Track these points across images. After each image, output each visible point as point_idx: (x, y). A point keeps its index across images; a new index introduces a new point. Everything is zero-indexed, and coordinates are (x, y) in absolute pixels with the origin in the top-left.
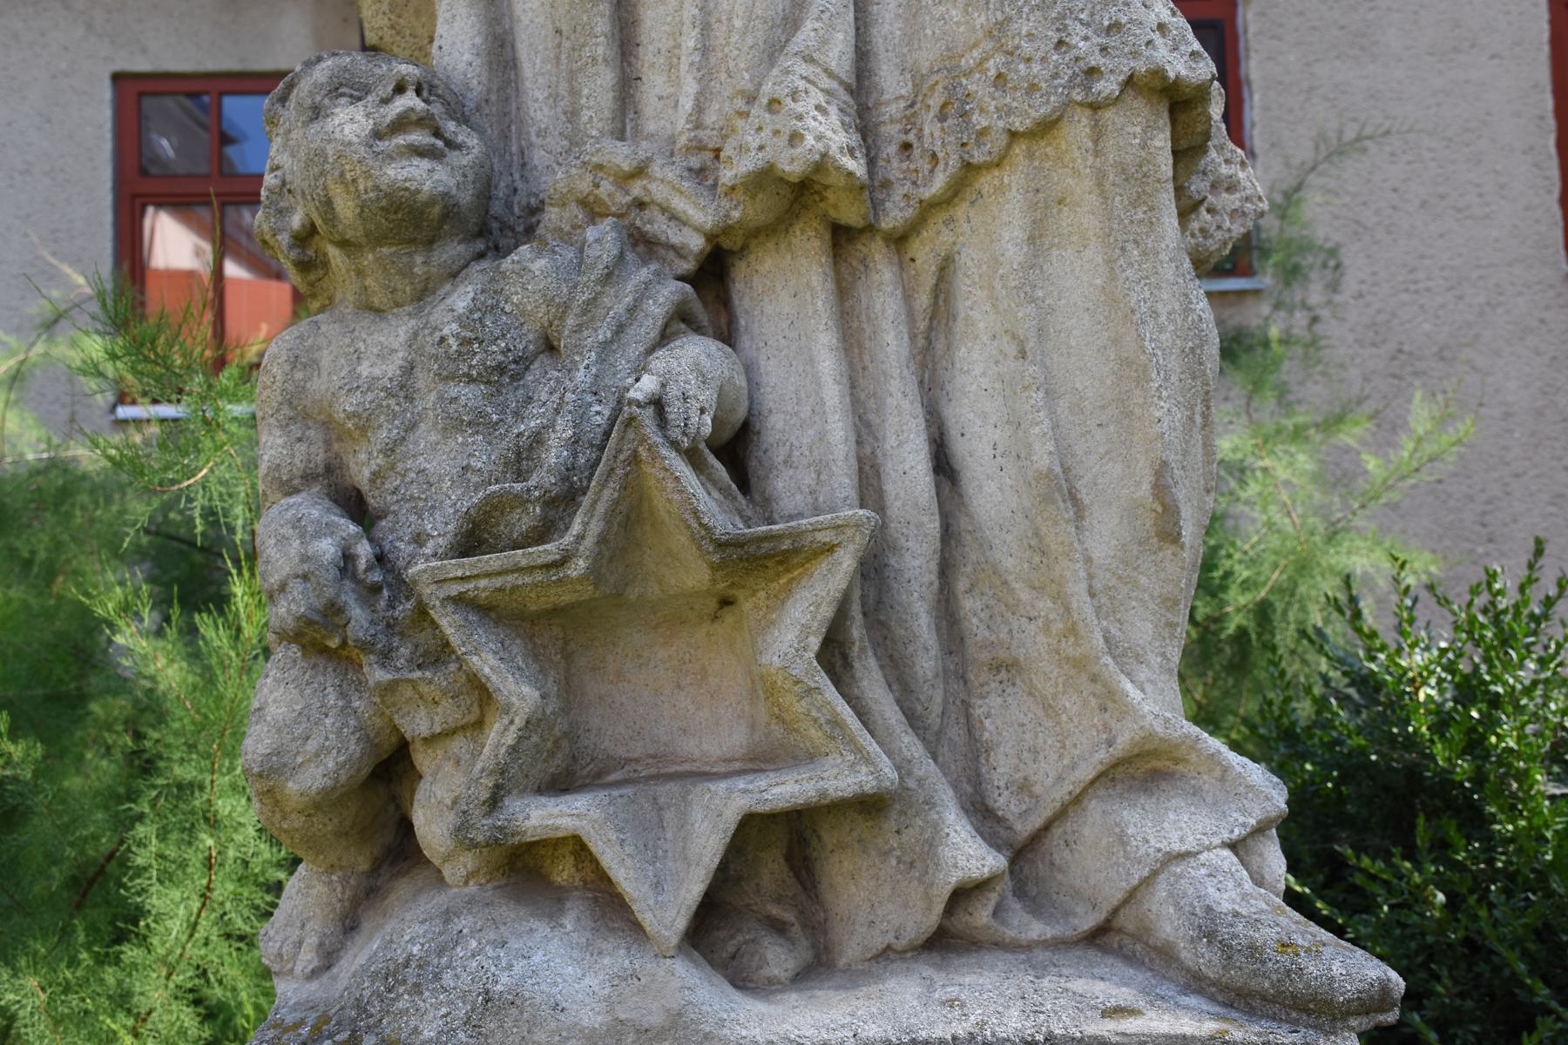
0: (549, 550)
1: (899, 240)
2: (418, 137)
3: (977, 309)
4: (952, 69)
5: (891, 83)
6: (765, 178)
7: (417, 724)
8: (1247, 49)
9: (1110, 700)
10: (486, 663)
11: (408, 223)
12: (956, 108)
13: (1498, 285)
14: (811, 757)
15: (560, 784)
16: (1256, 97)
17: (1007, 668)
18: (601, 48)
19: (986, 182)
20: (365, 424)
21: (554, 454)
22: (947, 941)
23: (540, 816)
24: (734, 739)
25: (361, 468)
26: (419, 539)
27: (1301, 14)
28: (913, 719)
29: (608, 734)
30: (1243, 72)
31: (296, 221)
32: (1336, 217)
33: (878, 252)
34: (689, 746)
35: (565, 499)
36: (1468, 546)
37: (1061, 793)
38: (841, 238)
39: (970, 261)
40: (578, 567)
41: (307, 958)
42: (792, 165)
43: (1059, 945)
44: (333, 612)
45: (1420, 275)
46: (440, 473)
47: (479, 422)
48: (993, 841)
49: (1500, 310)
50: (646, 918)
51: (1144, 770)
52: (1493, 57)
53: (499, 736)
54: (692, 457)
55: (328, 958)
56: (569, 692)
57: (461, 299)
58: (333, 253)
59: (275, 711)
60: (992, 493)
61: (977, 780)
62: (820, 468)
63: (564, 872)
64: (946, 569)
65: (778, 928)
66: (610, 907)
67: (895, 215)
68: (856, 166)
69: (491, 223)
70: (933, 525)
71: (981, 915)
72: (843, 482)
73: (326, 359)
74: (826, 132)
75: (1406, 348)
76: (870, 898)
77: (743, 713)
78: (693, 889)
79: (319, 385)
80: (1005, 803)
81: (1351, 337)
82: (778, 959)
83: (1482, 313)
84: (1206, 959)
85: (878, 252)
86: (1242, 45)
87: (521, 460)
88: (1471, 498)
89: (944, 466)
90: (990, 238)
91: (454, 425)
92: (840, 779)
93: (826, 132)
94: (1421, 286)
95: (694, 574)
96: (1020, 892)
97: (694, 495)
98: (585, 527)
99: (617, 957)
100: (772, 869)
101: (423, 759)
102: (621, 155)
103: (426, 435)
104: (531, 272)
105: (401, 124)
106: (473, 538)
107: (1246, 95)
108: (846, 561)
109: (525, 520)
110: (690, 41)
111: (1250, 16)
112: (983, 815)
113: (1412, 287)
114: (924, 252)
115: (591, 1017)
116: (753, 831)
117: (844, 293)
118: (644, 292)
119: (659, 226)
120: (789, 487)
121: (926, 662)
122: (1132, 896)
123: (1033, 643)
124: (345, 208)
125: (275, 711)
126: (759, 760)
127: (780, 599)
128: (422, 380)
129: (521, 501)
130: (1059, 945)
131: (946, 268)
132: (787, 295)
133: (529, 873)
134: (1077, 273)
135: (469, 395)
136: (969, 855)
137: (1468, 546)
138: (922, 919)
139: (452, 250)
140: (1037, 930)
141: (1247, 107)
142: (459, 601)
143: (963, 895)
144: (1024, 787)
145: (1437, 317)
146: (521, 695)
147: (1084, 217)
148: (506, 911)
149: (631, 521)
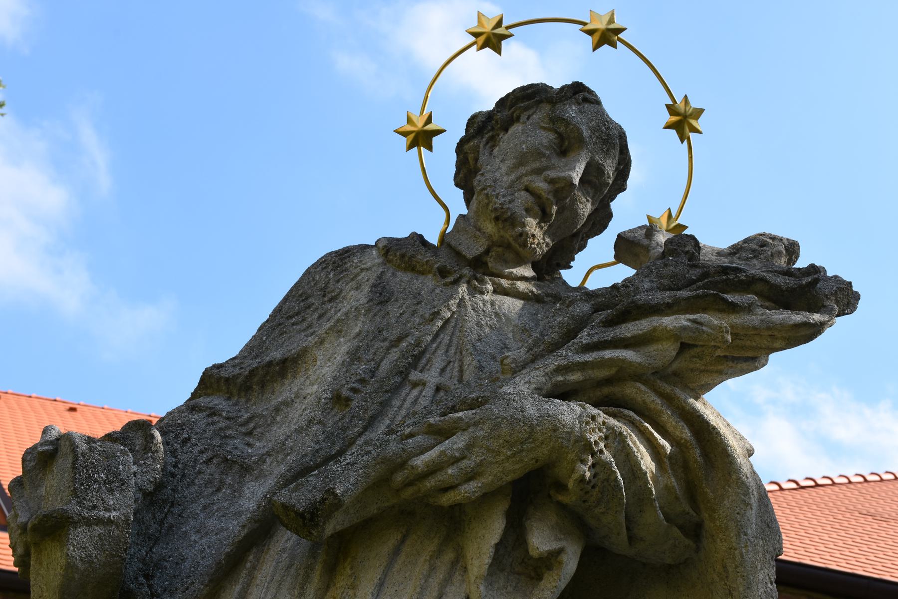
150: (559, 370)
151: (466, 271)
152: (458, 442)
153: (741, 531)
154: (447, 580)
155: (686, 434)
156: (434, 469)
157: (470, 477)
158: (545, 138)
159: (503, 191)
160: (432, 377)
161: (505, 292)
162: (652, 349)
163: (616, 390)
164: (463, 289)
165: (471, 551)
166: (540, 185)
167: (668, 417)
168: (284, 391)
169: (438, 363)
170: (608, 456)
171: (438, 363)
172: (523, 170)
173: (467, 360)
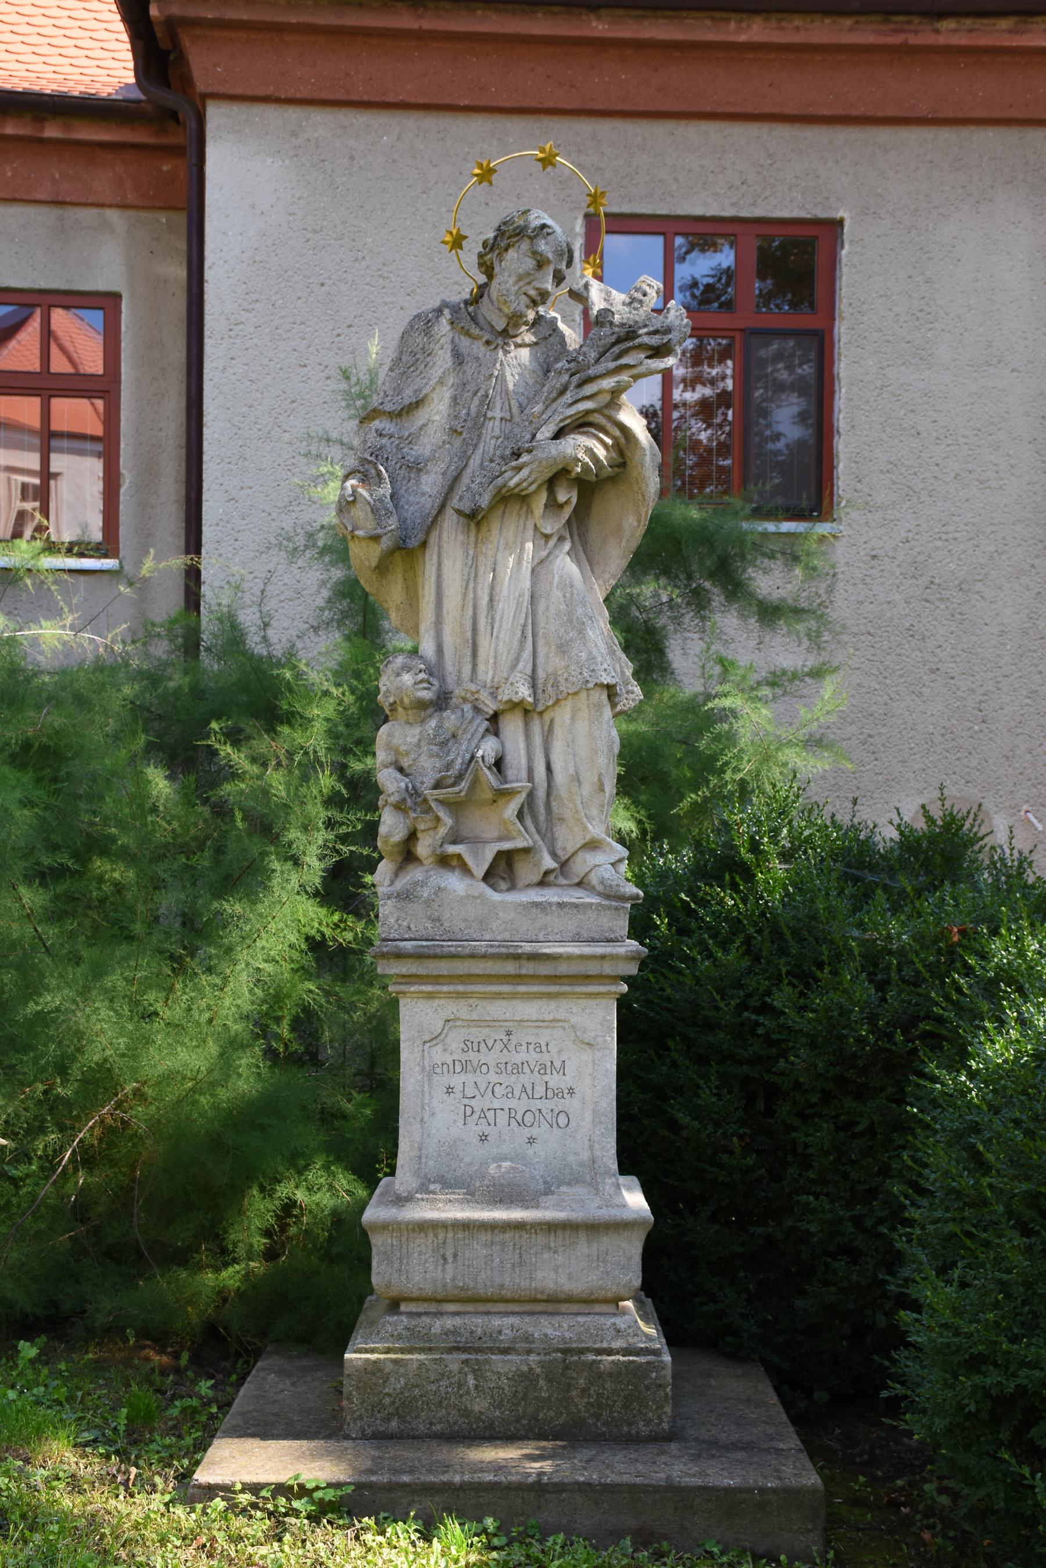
0: (457, 789)
1: (541, 713)
2: (425, 685)
3: (559, 732)
4: (555, 674)
5: (541, 674)
6: (510, 701)
7: (421, 826)
8: (840, 354)
9: (585, 829)
10: (441, 814)
11: (422, 705)
12: (556, 685)
13: (1004, 538)
14: (513, 839)
15: (454, 842)
16: (843, 391)
17: (561, 820)
18: (469, 659)
19: (562, 703)
20: (407, 753)
21: (457, 766)
22: (542, 883)
23: (452, 849)
24: (495, 834)
25: (405, 763)
26: (422, 783)
27: (880, 330)
28: (538, 831)
29: (465, 832)
30: (836, 372)
31: (391, 700)
32: (894, 483)
33: (536, 716)
34: (484, 835)
35: (460, 777)
36: (969, 724)
37: (571, 851)
38: (526, 712)
39: (557, 720)
40: (463, 794)
41: (387, 882)
42: (516, 699)
43: (569, 886)
44: (404, 800)
45: (951, 528)
46: (428, 768)
47: (437, 756)
48: (556, 861)
49: (1004, 557)
50: (475, 873)
51: (592, 845)
52: (1013, 370)
53: (442, 831)
54: (489, 768)
55: (392, 883)
56: (457, 821)
57: (433, 723)
58: (400, 709)
59: (389, 822)
60: (560, 778)
61: (553, 847)
62: (519, 770)
63: (454, 863)
64: (548, 795)
65: (503, 879)
66: (465, 870)
67: (540, 708)
68: (530, 700)
69: (442, 702)
70: (545, 785)
71: (552, 877)
72: (524, 774)
73: (397, 734)
74: (524, 692)
75: (937, 581)
76: (526, 872)
77: (498, 828)
78: (486, 867)
79: (395, 741)
80: (559, 852)
81: (898, 571)
82: (503, 885)
83: (991, 558)
84: (600, 888)
85: (536, 716)
86: (836, 350)
87: (448, 766)
88: (973, 691)
89: (549, 769)
90: (562, 716)
91: (431, 756)
92: (520, 844)
93: (524, 692)
94: (950, 536)
95: (489, 795)
96: (562, 874)
97: (489, 777)
98: (464, 785)
99: (468, 881)
100: (502, 865)
101: (420, 835)
102: (473, 687)
103: (423, 758)
104: (450, 719)
105: (421, 681)
106: (437, 786)
107: (837, 388)
108: (524, 795)
109: (450, 781)
110: (492, 661)
111: (842, 330)
112: (554, 855)
113: (944, 537)
114: (547, 717)
115: (462, 893)
116: (500, 854)
117: (527, 724)
118: (479, 726)
119: (481, 706)
120: (511, 774)
121: (542, 818)
122: (587, 874)
123: (568, 814)
124: (406, 701)
125: (389, 822)
126: (500, 839)
127: (509, 801)
128: (423, 743)
129: (449, 777)
130: (569, 886)
131: (552, 721)
132: (512, 727)
133: (444, 861)
134: (582, 726)
135: (435, 749)
136: (548, 863)
137: (969, 724)
138: (537, 878)
139: (431, 710)
140: (565, 882)
141: (837, 396)
142: (436, 800)
143: (547, 873)
144: (564, 849)
145: (960, 559)
146: (448, 821)
147: (584, 713)
148: (441, 870)
149: (475, 783)
150: (561, 421)
151: (500, 341)
152: (525, 472)
153: (643, 465)
154: (526, 519)
155: (617, 433)
156: (517, 485)
157: (531, 484)
158: (530, 263)
159: (513, 298)
160: (497, 413)
161: (520, 346)
162: (599, 398)
163: (586, 419)
164: (501, 353)
165: (534, 506)
166: (533, 293)
167: (609, 427)
168: (421, 417)
169: (498, 405)
170: (587, 460)
171: (498, 405)
172: (522, 283)
173: (513, 402)
